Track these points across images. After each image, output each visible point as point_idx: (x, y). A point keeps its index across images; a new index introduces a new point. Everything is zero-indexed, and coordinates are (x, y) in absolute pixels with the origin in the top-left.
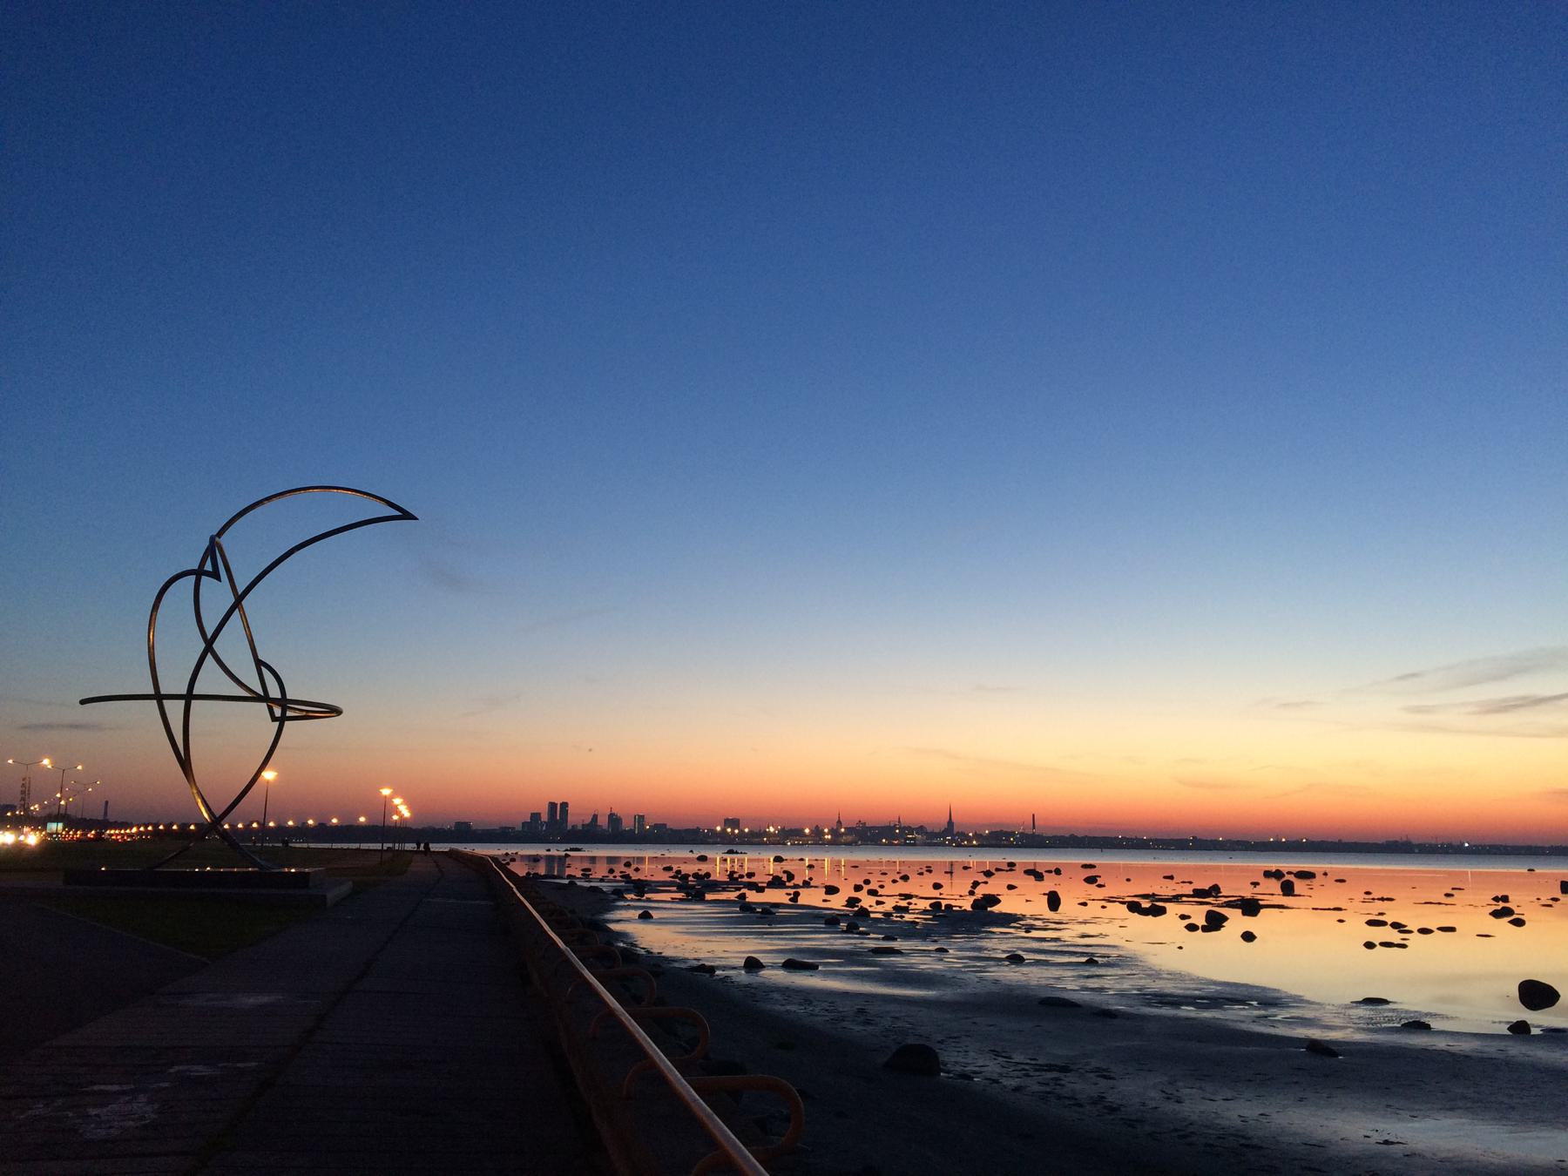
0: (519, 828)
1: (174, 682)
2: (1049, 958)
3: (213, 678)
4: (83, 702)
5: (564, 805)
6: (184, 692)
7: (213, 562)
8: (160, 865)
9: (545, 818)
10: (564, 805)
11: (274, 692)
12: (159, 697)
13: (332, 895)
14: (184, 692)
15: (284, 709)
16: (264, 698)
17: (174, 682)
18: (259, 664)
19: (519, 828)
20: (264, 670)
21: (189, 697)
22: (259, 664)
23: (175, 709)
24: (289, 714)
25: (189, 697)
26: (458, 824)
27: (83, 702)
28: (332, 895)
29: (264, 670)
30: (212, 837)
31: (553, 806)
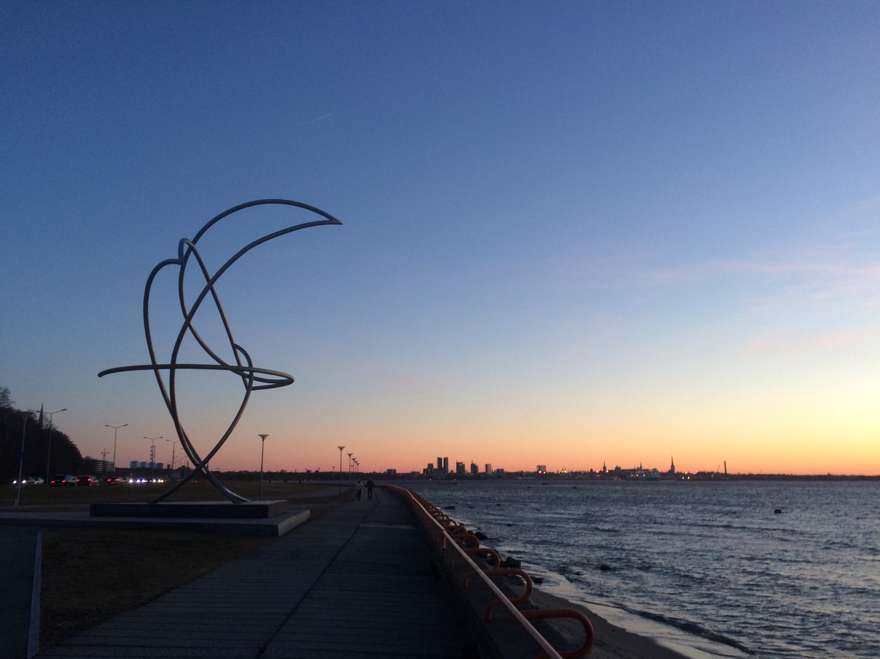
0: (422, 472)
1: (163, 358)
2: (331, 482)
3: (190, 352)
4: (101, 375)
5: (446, 459)
6: (169, 362)
7: (185, 254)
8: (160, 500)
9: (435, 466)
10: (446, 459)
11: (244, 363)
12: (155, 367)
13: (283, 526)
14: (169, 362)
15: (248, 375)
16: (238, 370)
17: (163, 358)
18: (235, 347)
19: (422, 472)
20: (239, 353)
21: (173, 367)
22: (235, 347)
23: (165, 374)
24: (256, 384)
25: (173, 367)
26: (389, 471)
27: (101, 375)
28: (283, 526)
29: (239, 353)
30: (198, 476)
31: (440, 460)
